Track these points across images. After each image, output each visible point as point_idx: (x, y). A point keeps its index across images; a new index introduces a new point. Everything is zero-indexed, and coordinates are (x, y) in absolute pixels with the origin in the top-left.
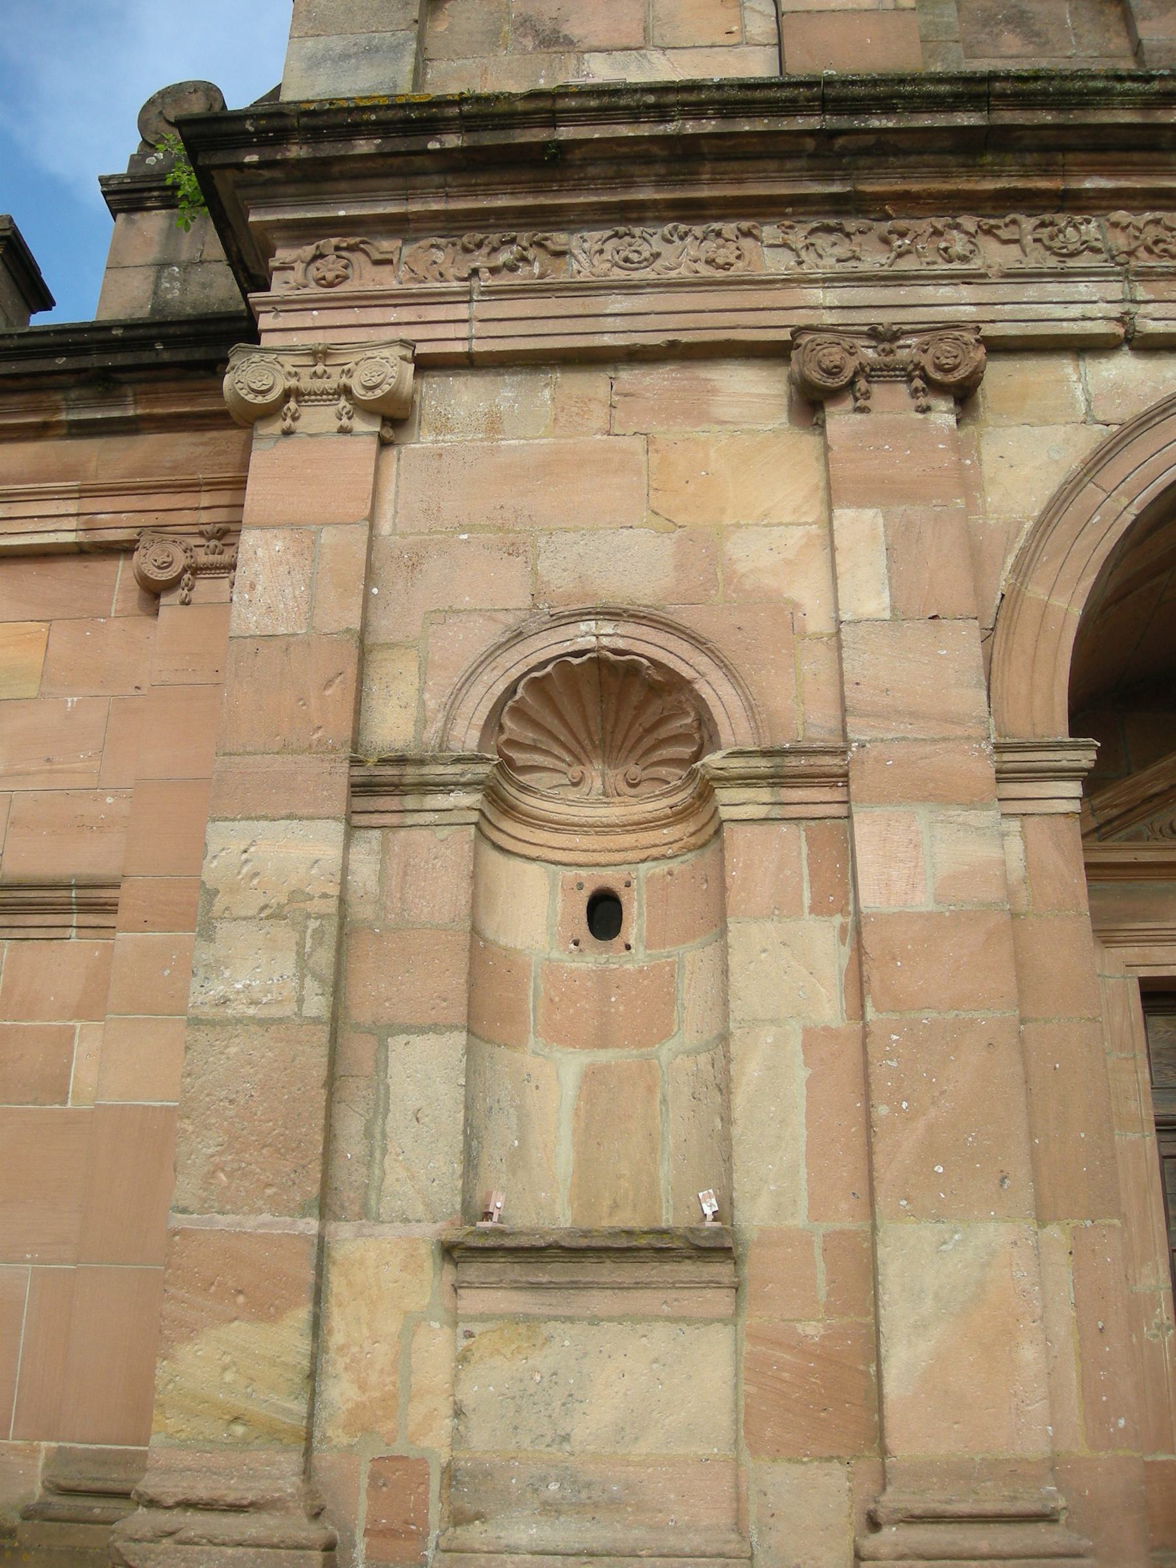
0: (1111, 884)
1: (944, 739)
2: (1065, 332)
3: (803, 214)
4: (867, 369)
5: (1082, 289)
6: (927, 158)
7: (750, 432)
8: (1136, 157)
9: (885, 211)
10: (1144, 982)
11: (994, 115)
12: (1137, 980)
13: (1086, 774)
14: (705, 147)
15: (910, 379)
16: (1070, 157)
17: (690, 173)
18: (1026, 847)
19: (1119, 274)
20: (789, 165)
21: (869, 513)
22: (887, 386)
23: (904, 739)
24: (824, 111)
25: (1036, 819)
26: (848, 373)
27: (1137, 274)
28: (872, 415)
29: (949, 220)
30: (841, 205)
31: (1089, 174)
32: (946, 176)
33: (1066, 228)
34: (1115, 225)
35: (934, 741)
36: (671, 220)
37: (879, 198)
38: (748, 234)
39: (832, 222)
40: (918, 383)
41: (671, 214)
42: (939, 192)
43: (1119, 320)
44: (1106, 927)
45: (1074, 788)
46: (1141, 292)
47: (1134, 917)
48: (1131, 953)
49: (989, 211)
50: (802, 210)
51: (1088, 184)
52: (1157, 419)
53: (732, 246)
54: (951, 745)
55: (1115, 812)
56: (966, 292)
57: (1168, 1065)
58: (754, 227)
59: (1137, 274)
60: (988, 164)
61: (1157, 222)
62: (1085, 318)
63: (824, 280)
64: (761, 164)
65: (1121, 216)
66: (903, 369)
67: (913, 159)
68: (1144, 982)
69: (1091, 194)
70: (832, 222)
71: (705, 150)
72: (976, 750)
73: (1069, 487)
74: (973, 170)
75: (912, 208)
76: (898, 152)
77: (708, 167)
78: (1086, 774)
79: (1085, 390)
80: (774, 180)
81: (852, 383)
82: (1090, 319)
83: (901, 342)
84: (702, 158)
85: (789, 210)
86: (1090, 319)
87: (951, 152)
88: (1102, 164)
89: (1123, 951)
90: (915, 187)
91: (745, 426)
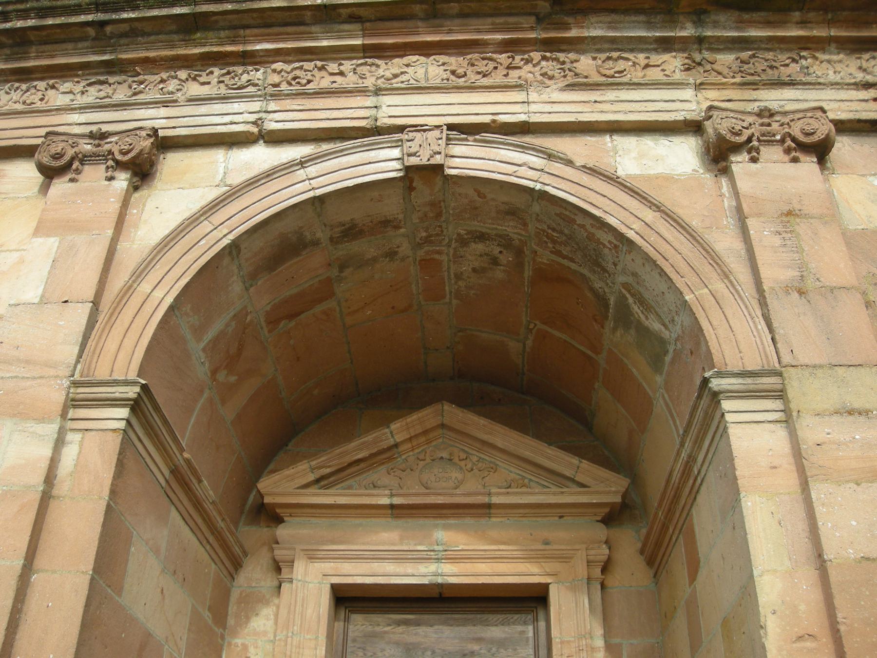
0: (324, 519)
1: (41, 377)
2: (217, 131)
3: (88, 74)
4: (80, 156)
5: (236, 107)
6: (161, 37)
7: (14, 198)
8: (289, 29)
9: (136, 70)
10: (335, 588)
11: (197, 7)
12: (329, 586)
13: (132, 402)
14: (32, 36)
15: (107, 160)
16: (248, 32)
17: (25, 53)
18: (80, 452)
19: (260, 96)
20: (80, 45)
21: (52, 239)
22: (94, 166)
23: (16, 377)
24: (97, 11)
25: (93, 433)
26: (67, 158)
27: (272, 95)
28: (78, 183)
29: (173, 73)
30: (111, 68)
31: (260, 42)
32: (173, 47)
33: (241, 75)
34: (274, 71)
35: (34, 378)
36: (8, 81)
37: (133, 62)
38: (53, 87)
39: (102, 78)
40: (110, 163)
41: (13, 78)
42: (166, 56)
43: (254, 123)
44: (310, 547)
45: (124, 412)
46: (272, 106)
47: (333, 542)
48: (327, 566)
49: (199, 68)
50: (87, 72)
51: (258, 47)
52: (263, 181)
53: (40, 93)
54: (43, 381)
55: (328, 470)
56: (163, 112)
57: (359, 648)
58: (56, 83)
59: (272, 95)
60: (198, 39)
61: (301, 68)
62: (232, 123)
63: (81, 108)
64: (64, 46)
65: (278, 66)
66: (103, 156)
67: (153, 38)
68: (335, 588)
69: (261, 54)
70: (102, 78)
71: (33, 38)
72: (58, 385)
73: (187, 222)
74: (188, 43)
75: (153, 68)
76: (144, 34)
77: (34, 48)
78: (132, 402)
79: (226, 168)
80: (72, 55)
81: (69, 165)
82: (235, 123)
83: (108, 140)
84: (31, 43)
85: (80, 72)
86: (235, 123)
87: (175, 33)
88: (268, 35)
89: (323, 565)
90: (152, 54)
91: (11, 195)
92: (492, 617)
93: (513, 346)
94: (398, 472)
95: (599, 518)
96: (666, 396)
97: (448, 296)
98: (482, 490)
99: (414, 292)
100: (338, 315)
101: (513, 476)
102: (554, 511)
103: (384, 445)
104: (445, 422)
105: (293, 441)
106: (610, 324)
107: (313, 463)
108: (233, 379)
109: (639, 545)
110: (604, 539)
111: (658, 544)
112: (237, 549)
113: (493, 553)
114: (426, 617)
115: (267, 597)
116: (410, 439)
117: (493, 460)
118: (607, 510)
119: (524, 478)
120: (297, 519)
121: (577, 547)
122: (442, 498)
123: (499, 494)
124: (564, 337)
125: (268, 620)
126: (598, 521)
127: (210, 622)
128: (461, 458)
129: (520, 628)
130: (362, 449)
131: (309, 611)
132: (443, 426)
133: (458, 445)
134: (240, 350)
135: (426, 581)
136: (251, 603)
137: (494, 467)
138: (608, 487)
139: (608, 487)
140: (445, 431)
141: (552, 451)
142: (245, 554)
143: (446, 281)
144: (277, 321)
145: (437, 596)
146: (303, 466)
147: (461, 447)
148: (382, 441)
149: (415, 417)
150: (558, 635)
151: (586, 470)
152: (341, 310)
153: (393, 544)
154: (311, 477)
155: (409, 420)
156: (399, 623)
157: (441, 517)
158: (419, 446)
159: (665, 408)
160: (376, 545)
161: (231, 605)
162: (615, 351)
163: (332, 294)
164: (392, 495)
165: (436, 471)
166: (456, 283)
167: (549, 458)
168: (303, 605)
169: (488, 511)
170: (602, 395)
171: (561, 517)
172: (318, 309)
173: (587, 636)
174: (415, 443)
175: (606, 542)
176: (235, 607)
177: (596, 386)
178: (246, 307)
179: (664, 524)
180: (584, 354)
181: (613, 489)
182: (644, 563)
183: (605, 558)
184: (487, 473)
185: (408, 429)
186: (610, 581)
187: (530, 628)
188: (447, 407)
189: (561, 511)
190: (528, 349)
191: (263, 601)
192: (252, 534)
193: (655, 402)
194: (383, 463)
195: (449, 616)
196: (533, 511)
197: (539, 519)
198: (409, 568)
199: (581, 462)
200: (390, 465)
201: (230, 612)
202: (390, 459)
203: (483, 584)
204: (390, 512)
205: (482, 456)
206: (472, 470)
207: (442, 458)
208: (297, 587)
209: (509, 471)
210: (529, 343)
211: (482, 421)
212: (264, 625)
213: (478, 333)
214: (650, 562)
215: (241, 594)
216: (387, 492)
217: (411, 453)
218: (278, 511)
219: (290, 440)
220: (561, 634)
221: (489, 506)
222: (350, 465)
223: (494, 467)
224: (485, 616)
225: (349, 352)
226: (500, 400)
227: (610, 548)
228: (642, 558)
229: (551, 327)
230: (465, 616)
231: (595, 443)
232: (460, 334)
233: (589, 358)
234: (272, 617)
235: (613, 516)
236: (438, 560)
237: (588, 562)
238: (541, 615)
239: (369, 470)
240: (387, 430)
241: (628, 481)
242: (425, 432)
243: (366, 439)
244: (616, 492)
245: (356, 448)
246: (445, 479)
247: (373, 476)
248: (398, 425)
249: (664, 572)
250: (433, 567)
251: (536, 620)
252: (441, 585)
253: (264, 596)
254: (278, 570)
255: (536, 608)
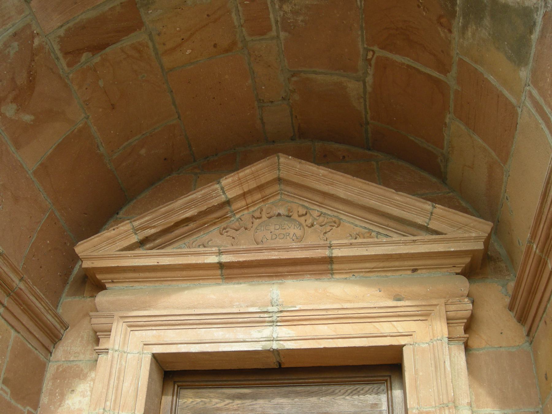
10: (156, 358)
12: (150, 356)
48: (150, 335)
55: (153, 231)
68: (156, 358)
89: (144, 333)
92: (337, 388)
93: (353, 87)
94: (231, 232)
95: (459, 270)
96: (535, 93)
97: (274, 28)
98: (322, 242)
99: (236, 23)
100: (153, 54)
101: (358, 229)
102: (406, 263)
103: (215, 202)
104: (281, 176)
105: (124, 210)
106: (458, 22)
107: (136, 224)
108: (28, 118)
109: (508, 300)
110: (466, 292)
111: (532, 292)
112: (49, 317)
113: (336, 312)
114: (264, 390)
115: (85, 371)
116: (244, 195)
117: (336, 214)
118: (468, 260)
119: (371, 231)
120: (120, 285)
121: (434, 302)
122: (276, 253)
123: (341, 246)
124: (406, 61)
125: (84, 396)
126: (457, 274)
127: (8, 397)
128: (300, 213)
129: (371, 398)
130: (190, 208)
131: (126, 384)
132: (279, 180)
133: (297, 201)
134: (32, 80)
135: (258, 347)
136: (69, 377)
137: (337, 220)
138: (466, 233)
139: (466, 233)
140: (282, 187)
141: (400, 198)
142: (66, 327)
143: (269, 5)
144: (78, 52)
145: (276, 366)
146: (125, 227)
147: (301, 203)
148: (212, 198)
149: (247, 171)
150: (415, 405)
151: (441, 216)
152: (154, 46)
153: (222, 307)
154: (134, 239)
155: (241, 174)
156: (234, 397)
157: (276, 276)
158: (254, 203)
159: (533, 111)
160: (206, 308)
161: (46, 382)
162: (466, 59)
163: (140, 25)
164: (220, 253)
165: (272, 228)
166: (281, 7)
167: (398, 206)
168: (119, 378)
169: (329, 267)
170: (455, 128)
171: (414, 270)
172: (127, 42)
173: (451, 405)
174: (249, 200)
175: (468, 296)
176: (50, 384)
177: (447, 121)
178: (29, 26)
179: (540, 260)
180: (429, 76)
181: (474, 235)
182: (515, 320)
183: (468, 314)
184: (330, 228)
185: (241, 184)
186: (475, 343)
187: (383, 398)
188: (283, 159)
189: (414, 263)
190: (369, 89)
191: (80, 375)
192: (71, 305)
193: (519, 110)
194: (215, 223)
195: (290, 389)
196: (382, 265)
197: (389, 274)
198: (240, 333)
199: (435, 207)
200: (224, 225)
201: (44, 390)
202: (223, 218)
203: (325, 349)
204: (219, 272)
205: (324, 211)
206: (312, 225)
207: (279, 215)
208: (113, 357)
209: (352, 223)
210: (369, 79)
211: (322, 171)
212: (80, 402)
213: (313, 76)
214: (522, 319)
215: (58, 369)
216: (215, 249)
217: (246, 212)
218: (99, 277)
219: (121, 208)
220: (418, 403)
221: (330, 260)
222: (177, 225)
223: (337, 220)
224: (332, 388)
225: (174, 103)
226: (344, 157)
227: (473, 302)
228: (512, 314)
229: (391, 51)
230: (308, 388)
231: (451, 194)
232: (294, 79)
233: (437, 81)
234: (89, 393)
235: (477, 267)
236: (273, 323)
237: (448, 319)
238: (396, 384)
239: (199, 231)
240: (217, 186)
241: (491, 224)
242: (260, 188)
243: (194, 196)
244: (476, 239)
245: (183, 206)
246: (282, 236)
247: (203, 237)
248: (230, 180)
249: (542, 324)
250: (267, 332)
251: (390, 388)
252: (277, 352)
253: (82, 370)
254: (97, 341)
255: (390, 377)
